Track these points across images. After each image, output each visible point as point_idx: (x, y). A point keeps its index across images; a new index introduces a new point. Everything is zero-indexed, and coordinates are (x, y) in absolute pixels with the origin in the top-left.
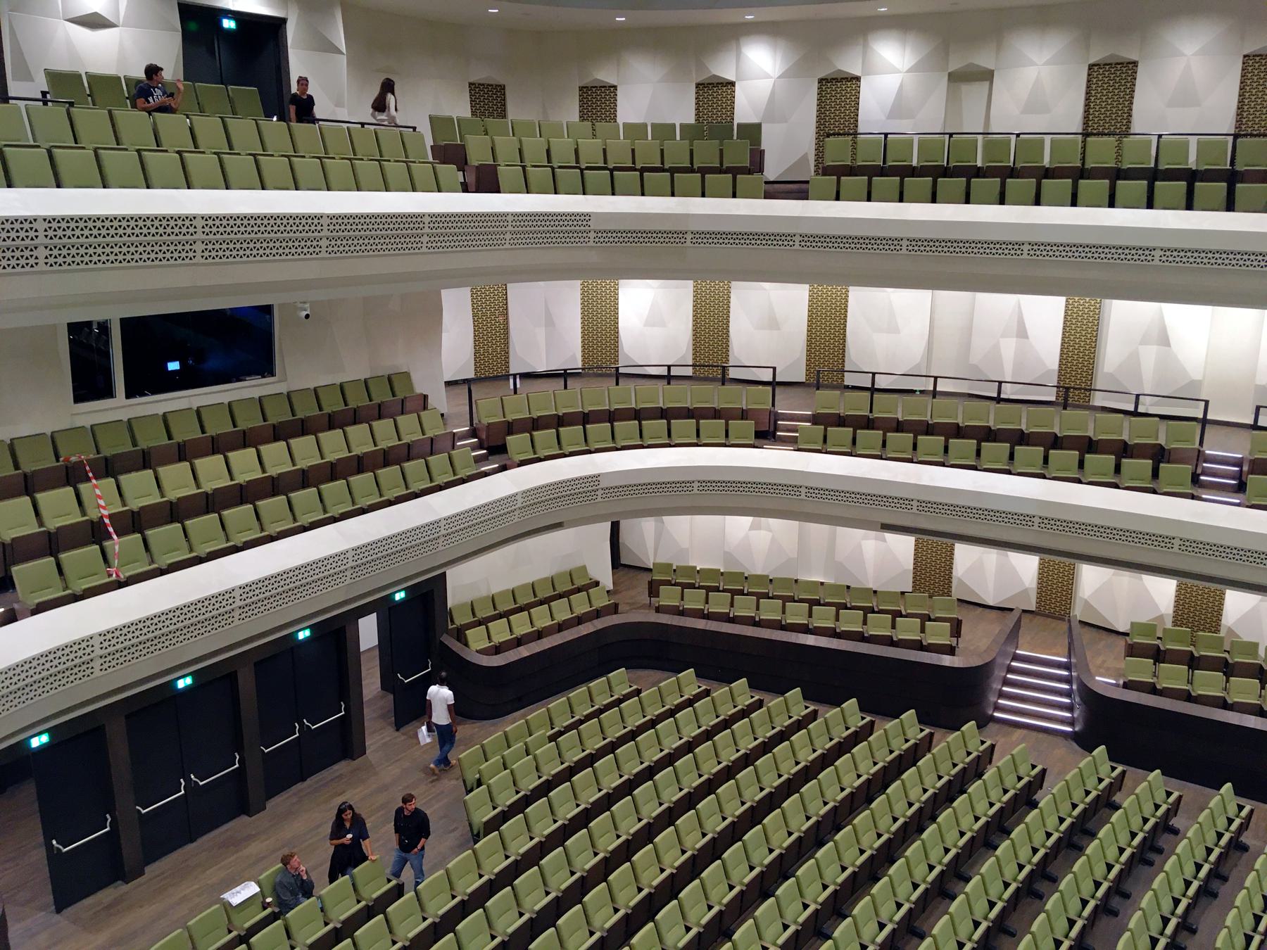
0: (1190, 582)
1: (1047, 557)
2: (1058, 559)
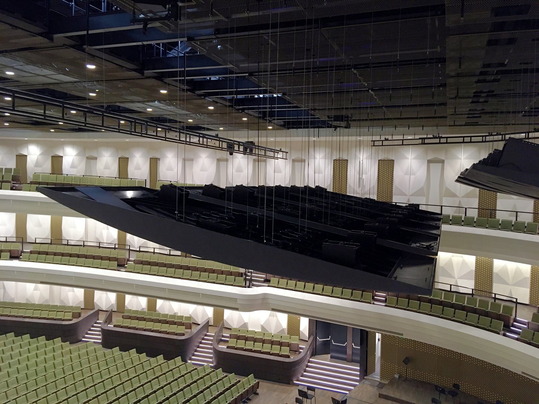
0: (120, 293)
1: (290, 314)
2: (89, 289)
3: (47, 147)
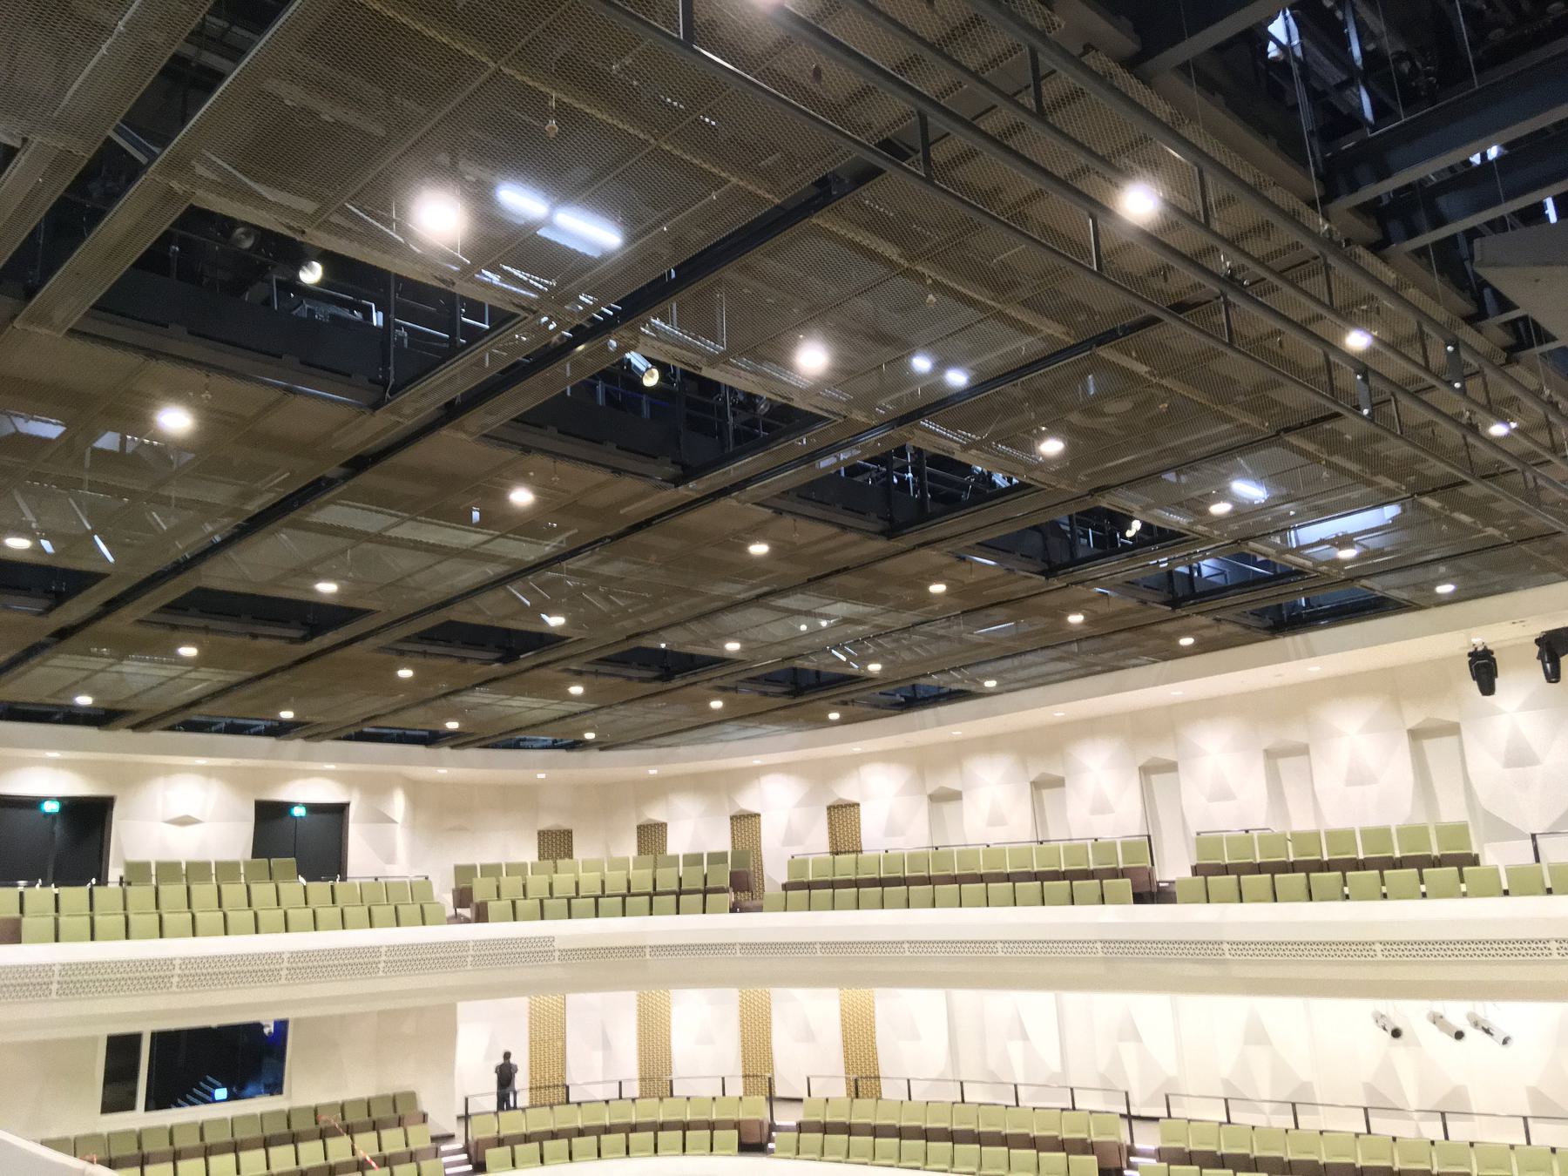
3: (821, 775)
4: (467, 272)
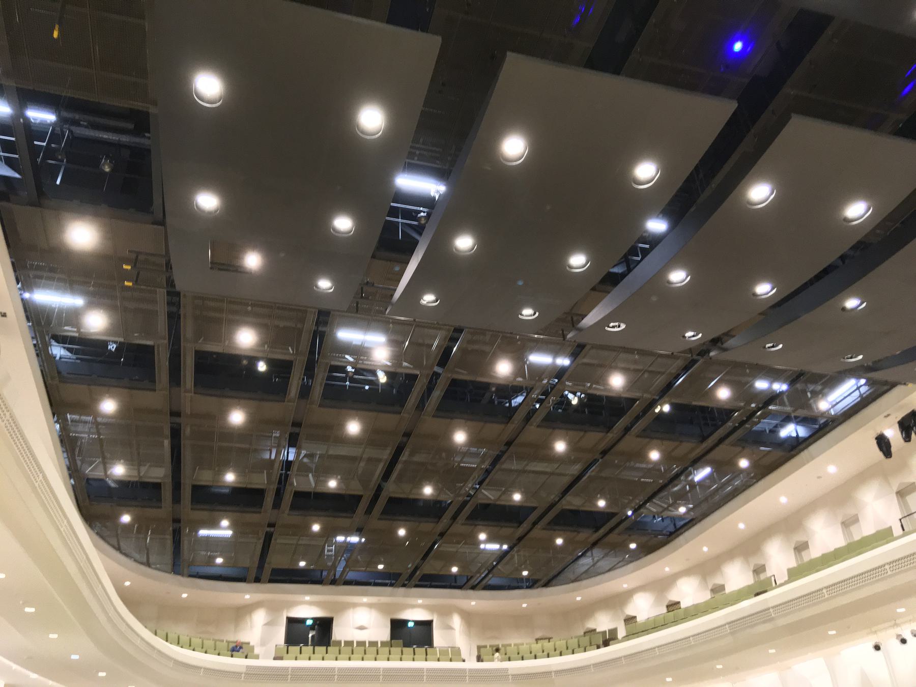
4: (515, 379)
